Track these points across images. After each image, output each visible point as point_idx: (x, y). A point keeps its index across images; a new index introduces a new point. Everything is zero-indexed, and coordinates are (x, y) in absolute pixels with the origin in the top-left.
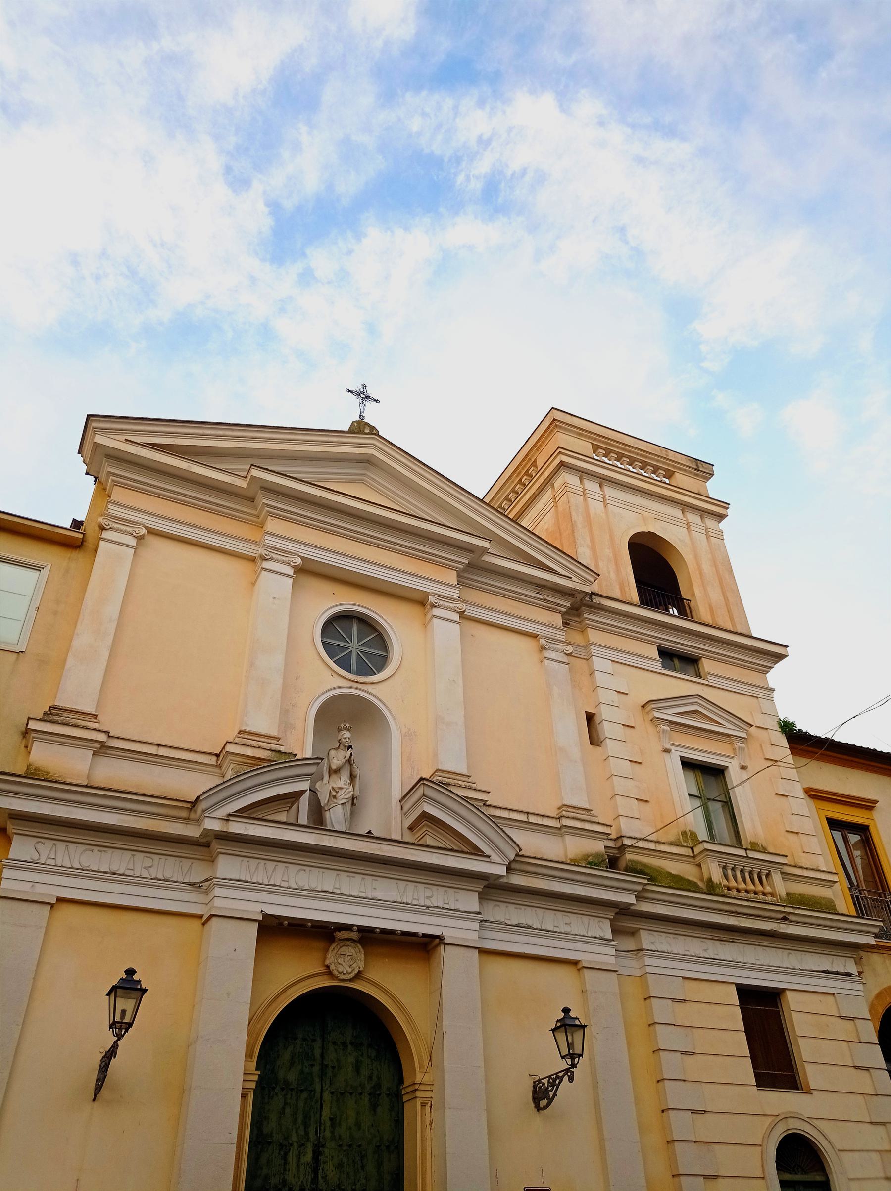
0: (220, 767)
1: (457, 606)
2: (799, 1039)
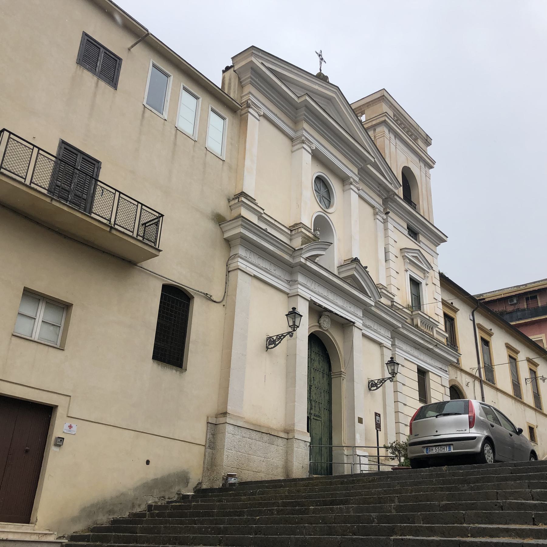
0: (291, 235)
1: (358, 186)
2: (431, 389)
